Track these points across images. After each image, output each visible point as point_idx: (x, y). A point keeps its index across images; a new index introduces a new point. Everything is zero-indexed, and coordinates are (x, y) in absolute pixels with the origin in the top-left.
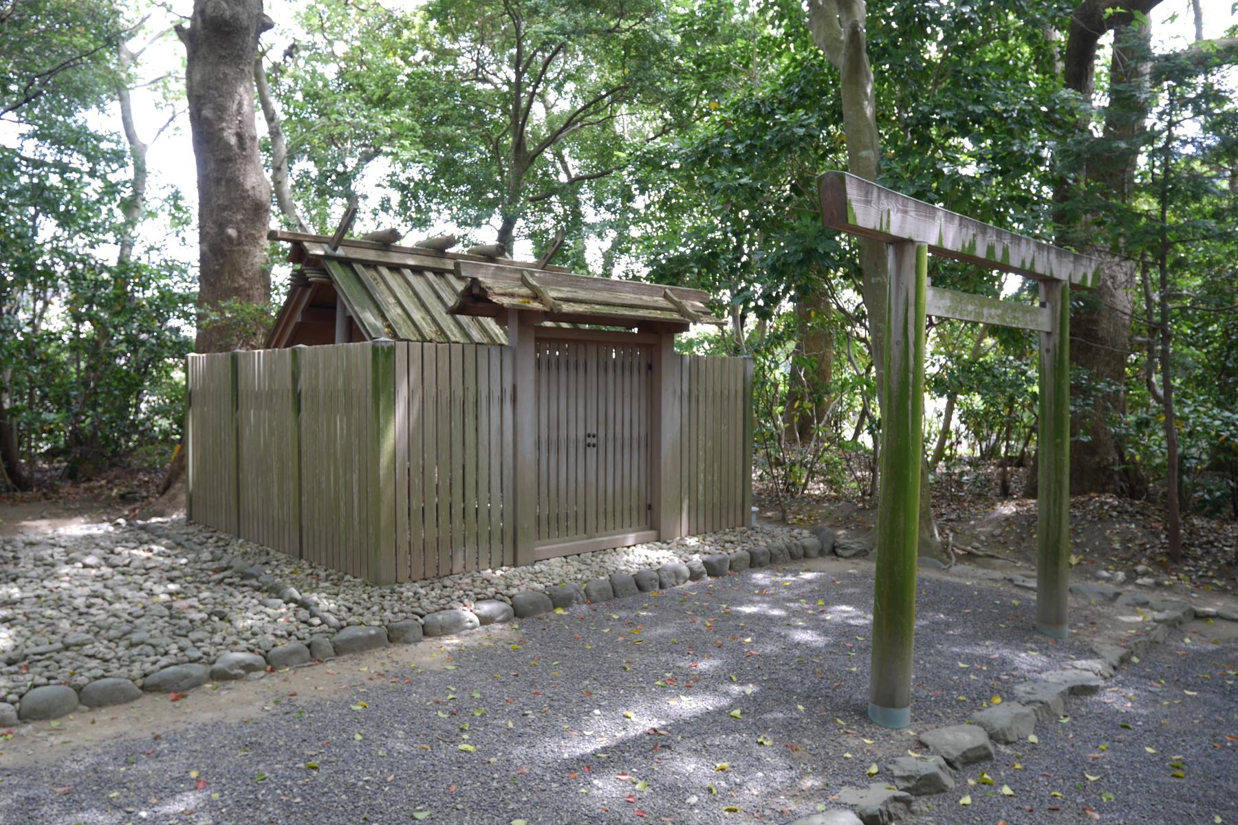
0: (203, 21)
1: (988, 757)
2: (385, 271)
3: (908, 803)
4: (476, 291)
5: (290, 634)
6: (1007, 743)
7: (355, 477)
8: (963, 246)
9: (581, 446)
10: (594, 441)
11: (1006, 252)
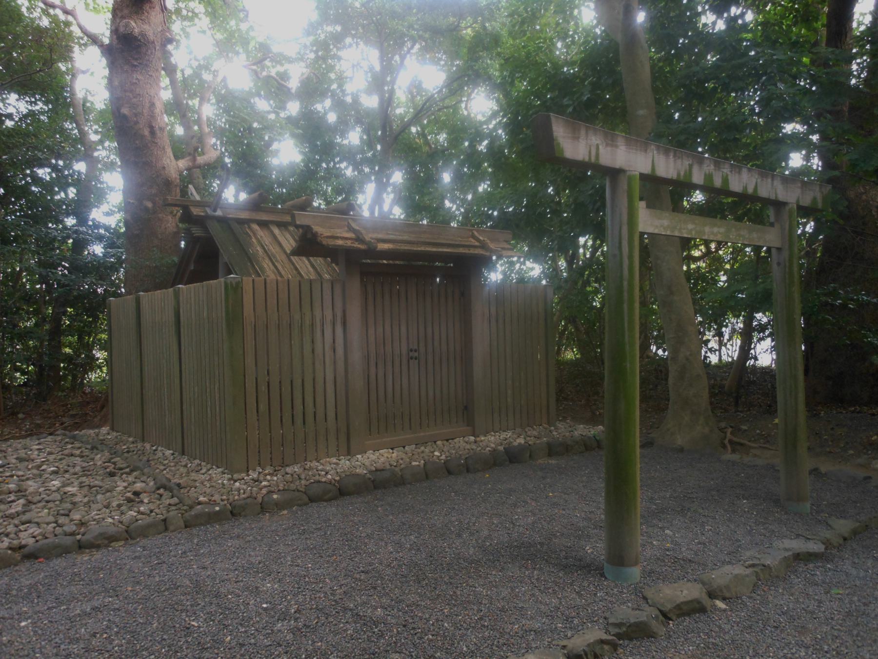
0: (118, 38)
1: (702, 610)
2: (255, 227)
3: (615, 647)
4: (309, 236)
5: (151, 511)
6: (724, 599)
7: (217, 386)
8: (679, 175)
9: (405, 361)
10: (416, 354)
11: (725, 180)
